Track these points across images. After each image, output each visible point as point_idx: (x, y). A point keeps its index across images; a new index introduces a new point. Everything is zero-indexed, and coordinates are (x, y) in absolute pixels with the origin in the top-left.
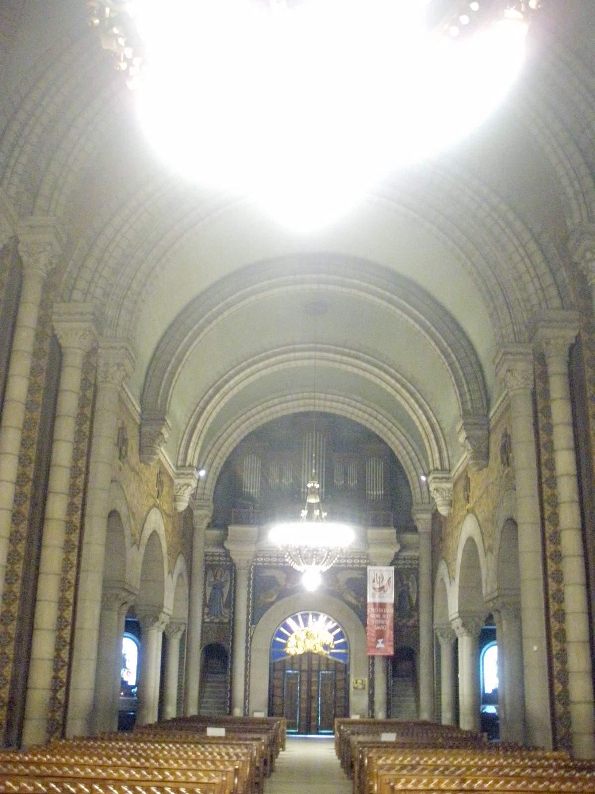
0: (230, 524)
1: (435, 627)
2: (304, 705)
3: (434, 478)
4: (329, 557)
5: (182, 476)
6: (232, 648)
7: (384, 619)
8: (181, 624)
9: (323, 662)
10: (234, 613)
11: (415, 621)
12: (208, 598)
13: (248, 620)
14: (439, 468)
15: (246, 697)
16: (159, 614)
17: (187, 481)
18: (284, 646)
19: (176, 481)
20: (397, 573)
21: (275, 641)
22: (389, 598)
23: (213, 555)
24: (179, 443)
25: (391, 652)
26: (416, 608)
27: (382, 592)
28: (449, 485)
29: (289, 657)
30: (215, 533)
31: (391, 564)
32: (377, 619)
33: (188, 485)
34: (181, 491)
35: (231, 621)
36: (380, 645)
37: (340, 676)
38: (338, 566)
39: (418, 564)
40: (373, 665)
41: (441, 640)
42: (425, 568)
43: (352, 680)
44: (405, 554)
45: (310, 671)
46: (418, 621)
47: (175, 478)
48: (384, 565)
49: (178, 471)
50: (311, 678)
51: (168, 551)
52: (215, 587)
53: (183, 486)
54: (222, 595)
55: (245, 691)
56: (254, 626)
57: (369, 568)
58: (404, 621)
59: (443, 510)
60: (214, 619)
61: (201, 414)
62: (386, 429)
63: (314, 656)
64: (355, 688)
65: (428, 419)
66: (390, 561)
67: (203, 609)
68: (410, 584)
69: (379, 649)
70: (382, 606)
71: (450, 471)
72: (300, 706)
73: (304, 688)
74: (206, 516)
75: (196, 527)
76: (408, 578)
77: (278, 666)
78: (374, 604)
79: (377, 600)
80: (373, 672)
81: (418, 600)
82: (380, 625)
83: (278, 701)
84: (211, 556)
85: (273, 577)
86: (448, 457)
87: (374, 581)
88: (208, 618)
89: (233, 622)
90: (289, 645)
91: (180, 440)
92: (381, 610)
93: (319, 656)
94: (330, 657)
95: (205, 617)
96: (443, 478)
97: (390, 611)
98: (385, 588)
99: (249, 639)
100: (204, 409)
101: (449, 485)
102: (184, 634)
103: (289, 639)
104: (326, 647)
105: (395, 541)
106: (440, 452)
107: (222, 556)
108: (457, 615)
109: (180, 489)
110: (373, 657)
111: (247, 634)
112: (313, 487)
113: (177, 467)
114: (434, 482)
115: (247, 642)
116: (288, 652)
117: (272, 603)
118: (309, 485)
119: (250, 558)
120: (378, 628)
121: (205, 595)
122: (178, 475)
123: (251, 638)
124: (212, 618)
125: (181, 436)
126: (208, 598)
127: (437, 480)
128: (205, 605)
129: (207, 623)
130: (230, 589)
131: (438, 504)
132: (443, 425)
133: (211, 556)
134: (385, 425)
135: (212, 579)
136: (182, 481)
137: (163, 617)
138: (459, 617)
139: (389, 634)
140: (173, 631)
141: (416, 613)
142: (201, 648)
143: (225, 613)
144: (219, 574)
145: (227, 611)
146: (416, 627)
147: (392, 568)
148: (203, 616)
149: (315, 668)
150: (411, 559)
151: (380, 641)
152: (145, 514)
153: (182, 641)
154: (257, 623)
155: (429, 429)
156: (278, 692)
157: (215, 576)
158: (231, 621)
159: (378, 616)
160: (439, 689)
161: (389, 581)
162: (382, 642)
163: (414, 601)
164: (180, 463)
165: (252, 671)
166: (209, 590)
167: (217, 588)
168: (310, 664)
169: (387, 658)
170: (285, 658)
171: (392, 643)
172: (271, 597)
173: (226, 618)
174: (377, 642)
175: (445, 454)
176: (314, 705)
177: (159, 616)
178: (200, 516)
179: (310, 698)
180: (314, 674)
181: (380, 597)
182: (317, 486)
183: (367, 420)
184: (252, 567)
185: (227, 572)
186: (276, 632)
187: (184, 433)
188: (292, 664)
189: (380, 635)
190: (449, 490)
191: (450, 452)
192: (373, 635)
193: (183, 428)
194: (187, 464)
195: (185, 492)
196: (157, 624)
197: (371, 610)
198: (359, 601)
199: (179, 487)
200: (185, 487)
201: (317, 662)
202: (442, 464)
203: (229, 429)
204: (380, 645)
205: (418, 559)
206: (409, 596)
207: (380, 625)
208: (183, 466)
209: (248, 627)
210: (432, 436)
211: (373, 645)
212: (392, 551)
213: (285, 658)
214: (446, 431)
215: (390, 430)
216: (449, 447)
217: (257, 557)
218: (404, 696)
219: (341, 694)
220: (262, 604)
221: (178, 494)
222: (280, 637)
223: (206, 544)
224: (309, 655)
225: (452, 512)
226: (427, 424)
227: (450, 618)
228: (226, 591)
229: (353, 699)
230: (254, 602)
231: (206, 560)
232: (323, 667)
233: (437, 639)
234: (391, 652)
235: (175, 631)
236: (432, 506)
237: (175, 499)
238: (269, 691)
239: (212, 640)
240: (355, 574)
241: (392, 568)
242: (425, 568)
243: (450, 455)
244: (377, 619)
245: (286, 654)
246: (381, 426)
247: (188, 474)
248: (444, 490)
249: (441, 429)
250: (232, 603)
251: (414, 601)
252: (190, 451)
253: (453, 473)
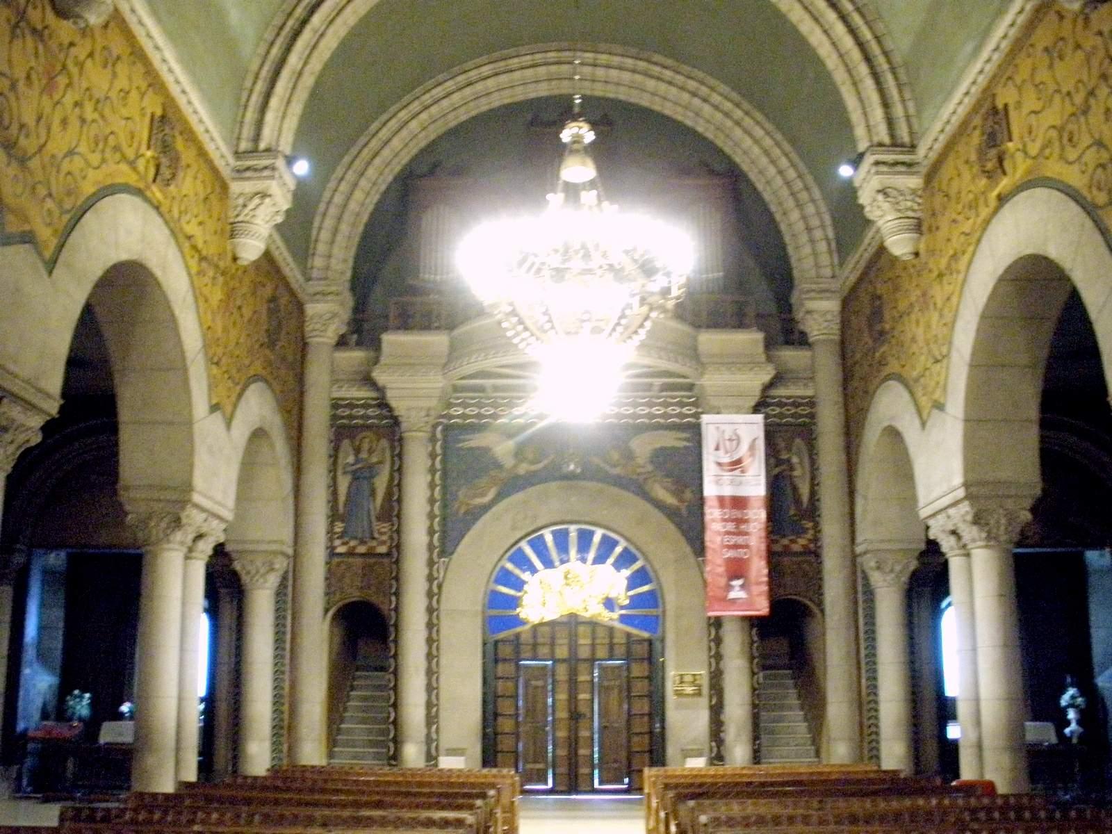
0: (386, 329)
1: (859, 549)
2: (562, 734)
3: (877, 163)
4: (623, 322)
5: (248, 174)
6: (397, 609)
7: (746, 534)
8: (275, 553)
9: (602, 638)
10: (398, 532)
11: (810, 540)
12: (342, 498)
13: (431, 547)
14: (887, 140)
15: (432, 719)
16: (183, 508)
17: (259, 185)
18: (514, 602)
19: (235, 187)
20: (771, 435)
21: (495, 594)
22: (755, 485)
23: (351, 406)
24: (244, 100)
25: (762, 607)
26: (812, 512)
27: (737, 472)
28: (915, 182)
29: (527, 627)
30: (354, 357)
31: (756, 409)
32: (728, 533)
33: (264, 195)
34: (246, 211)
35: (394, 550)
36: (736, 593)
37: (638, 670)
38: (631, 421)
39: (812, 416)
40: (718, 641)
41: (876, 578)
42: (829, 421)
43: (671, 674)
44: (781, 392)
45: (573, 662)
46: (816, 540)
47: (234, 179)
48: (738, 410)
49: (239, 163)
50: (576, 675)
51: (206, 346)
52: (356, 476)
53: (252, 198)
54: (373, 493)
55: (429, 705)
56: (446, 560)
57: (705, 418)
58: (785, 541)
59: (899, 245)
60: (354, 548)
61: (296, 34)
62: (729, 123)
63: (581, 629)
64: (679, 694)
65: (852, 31)
66: (753, 403)
67: (331, 524)
68: (795, 460)
69: (734, 601)
70: (739, 503)
71: (913, 147)
72: (553, 735)
73: (562, 696)
74: (334, 315)
75: (308, 340)
76: (789, 449)
77: (505, 651)
78: (721, 500)
79: (728, 491)
80: (718, 657)
81: (813, 494)
82: (736, 547)
83: (506, 725)
84: (346, 406)
85: (486, 451)
86: (908, 117)
87: (717, 449)
88: (344, 544)
89: (395, 553)
90: (526, 600)
91: (245, 95)
92: (737, 514)
93: (593, 624)
94: (618, 625)
95: (337, 542)
96: (896, 164)
97: (758, 515)
98: (745, 464)
99: (434, 594)
100: (304, 22)
101: (915, 182)
102: (284, 578)
103: (526, 587)
104: (609, 604)
105: (763, 358)
106: (886, 105)
107: (370, 406)
108: (961, 493)
109: (245, 206)
110: (717, 623)
111: (430, 579)
112: (577, 140)
113: (237, 154)
114: (877, 173)
115: (430, 595)
116: (522, 616)
117: (486, 508)
118: (566, 135)
119: (434, 403)
120: (731, 554)
121: (334, 493)
122: (240, 173)
123: (440, 587)
124: (352, 543)
125: (248, 84)
126: (342, 498)
127: (884, 169)
128: (334, 516)
129: (341, 554)
130: (391, 479)
131: (884, 231)
132: (889, 45)
133: (346, 406)
134: (727, 115)
135: (351, 459)
136: (248, 187)
137: (194, 519)
138: (967, 497)
139: (759, 568)
140: (257, 572)
141: (810, 525)
142: (326, 611)
143: (381, 534)
144: (366, 446)
145: (385, 527)
146: (814, 553)
147: (759, 418)
148: (331, 540)
149: (584, 653)
150: (796, 405)
151: (737, 583)
152: (88, 189)
153: (280, 593)
154: (452, 553)
155: (856, 55)
156: (505, 707)
157: (357, 451)
158: (394, 550)
159: (731, 527)
160: (873, 689)
161: (752, 447)
162: (743, 587)
163: (805, 498)
164: (244, 146)
165: (444, 661)
166: (344, 483)
167: (363, 475)
168: (573, 647)
169: (755, 623)
170: (519, 629)
171: (765, 588)
172: (483, 495)
173: (383, 543)
174: (729, 588)
175: (898, 111)
176: (584, 733)
177: (183, 515)
178: (321, 317)
179: (575, 716)
180: (583, 667)
181: (732, 482)
182: (589, 137)
183: (686, 108)
184: (440, 428)
185: (384, 443)
186: (495, 573)
187: (257, 77)
188: (535, 646)
189: (737, 570)
190: (914, 192)
191: (911, 105)
192: (721, 570)
193: (254, 67)
194: (262, 146)
195: (258, 212)
196: (178, 536)
197: (713, 514)
198: (681, 500)
199: (241, 201)
200: (256, 201)
201: (588, 641)
202: (892, 135)
203: (384, 130)
204: (736, 593)
205: (812, 403)
206: (795, 489)
207: (736, 547)
208: (255, 150)
209: (431, 563)
210: (863, 69)
211: (719, 593)
212: (754, 380)
213: (519, 629)
214: (897, 59)
215: (738, 123)
216: (907, 95)
217: (450, 406)
218: (782, 708)
219: (642, 706)
220: (462, 511)
221: (240, 219)
222: (505, 585)
223: (335, 381)
224: (572, 622)
225: (922, 248)
226: (848, 42)
227: (924, 513)
228: (381, 483)
229: (674, 715)
230: (444, 506)
231: (334, 418)
232: (602, 652)
233: (866, 578)
234: (762, 607)
235: (262, 571)
236: (841, 282)
237: (232, 231)
238: (485, 702)
239: (355, 595)
240: (671, 440)
241: (759, 418)
242: (829, 421)
243: (912, 111)
244: (728, 533)
245: (517, 621)
246: (719, 116)
247: (266, 168)
248: (901, 193)
249: (886, 54)
250: (393, 510)
251: (805, 498)
252: (270, 117)
253: (921, 151)
